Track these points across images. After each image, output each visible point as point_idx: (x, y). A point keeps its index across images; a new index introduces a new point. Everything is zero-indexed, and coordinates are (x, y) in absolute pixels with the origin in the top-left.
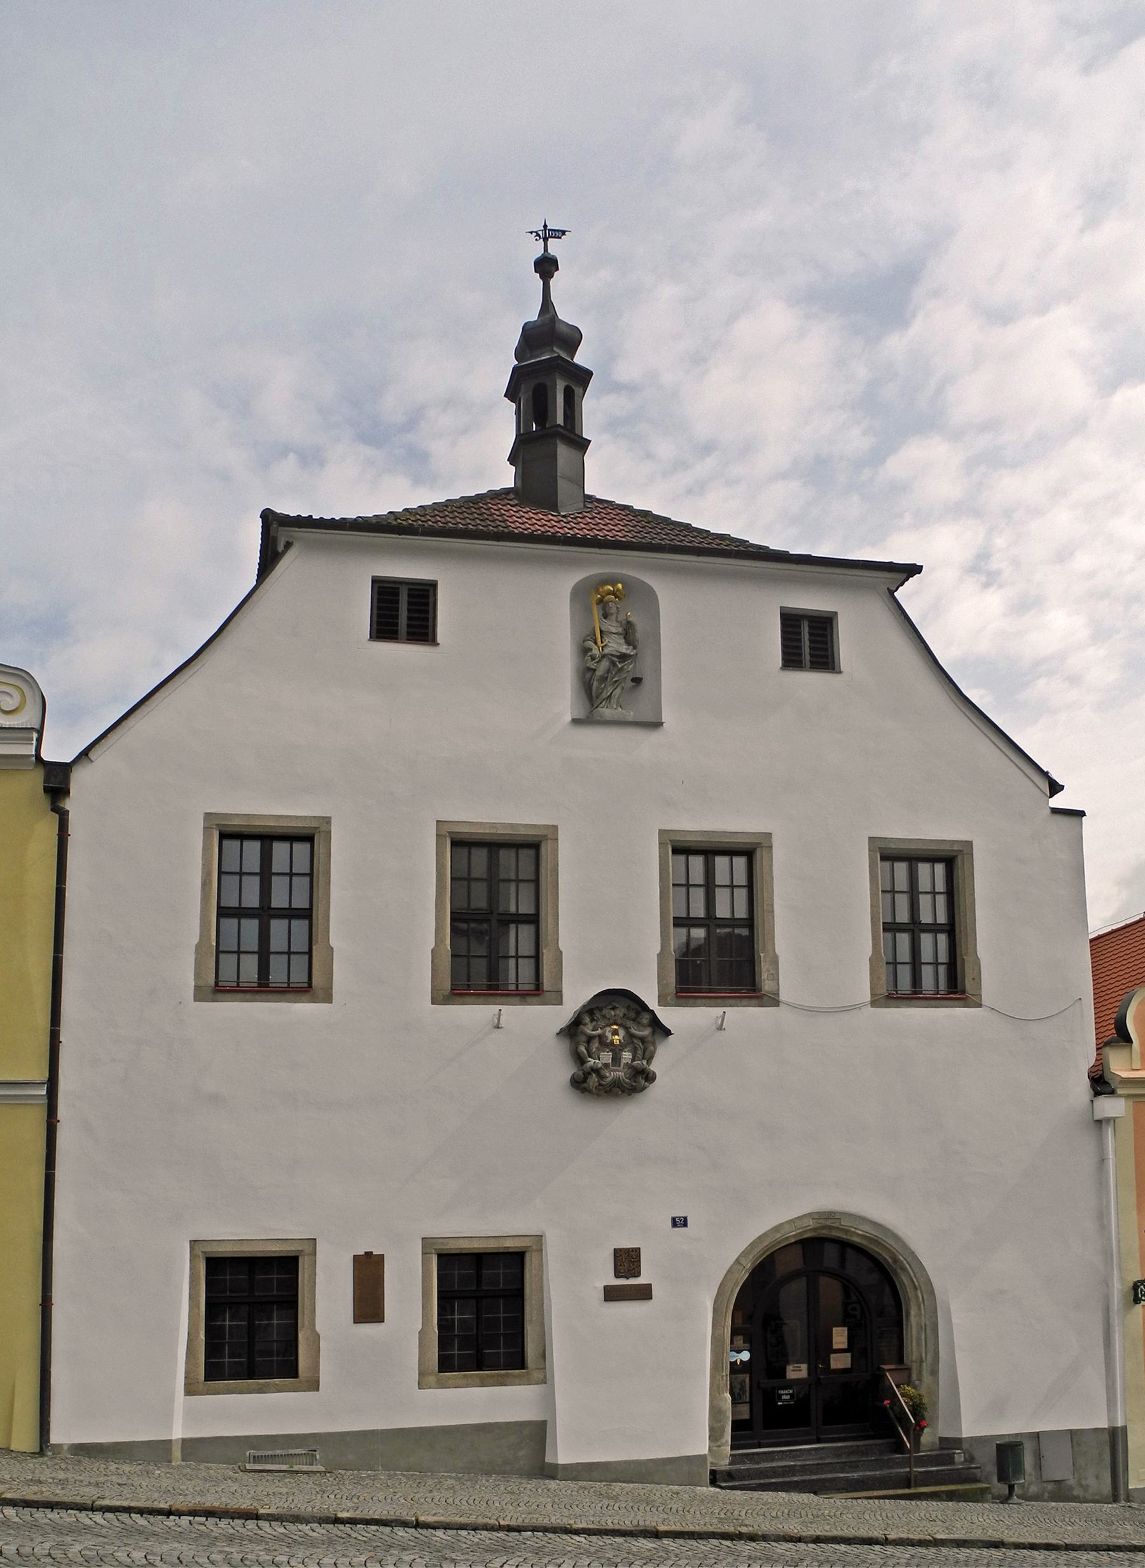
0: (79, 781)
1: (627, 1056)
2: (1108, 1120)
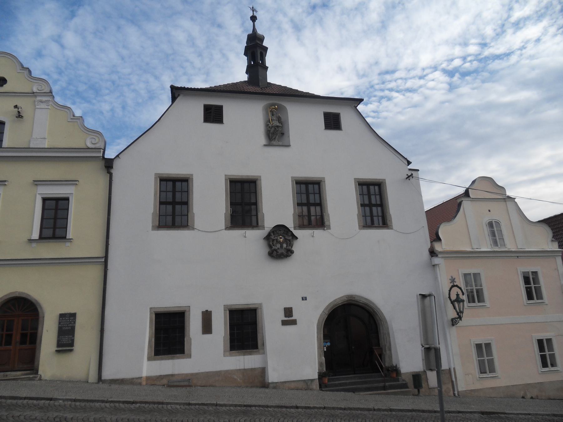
0: (116, 164)
1: (285, 245)
2: (436, 265)
